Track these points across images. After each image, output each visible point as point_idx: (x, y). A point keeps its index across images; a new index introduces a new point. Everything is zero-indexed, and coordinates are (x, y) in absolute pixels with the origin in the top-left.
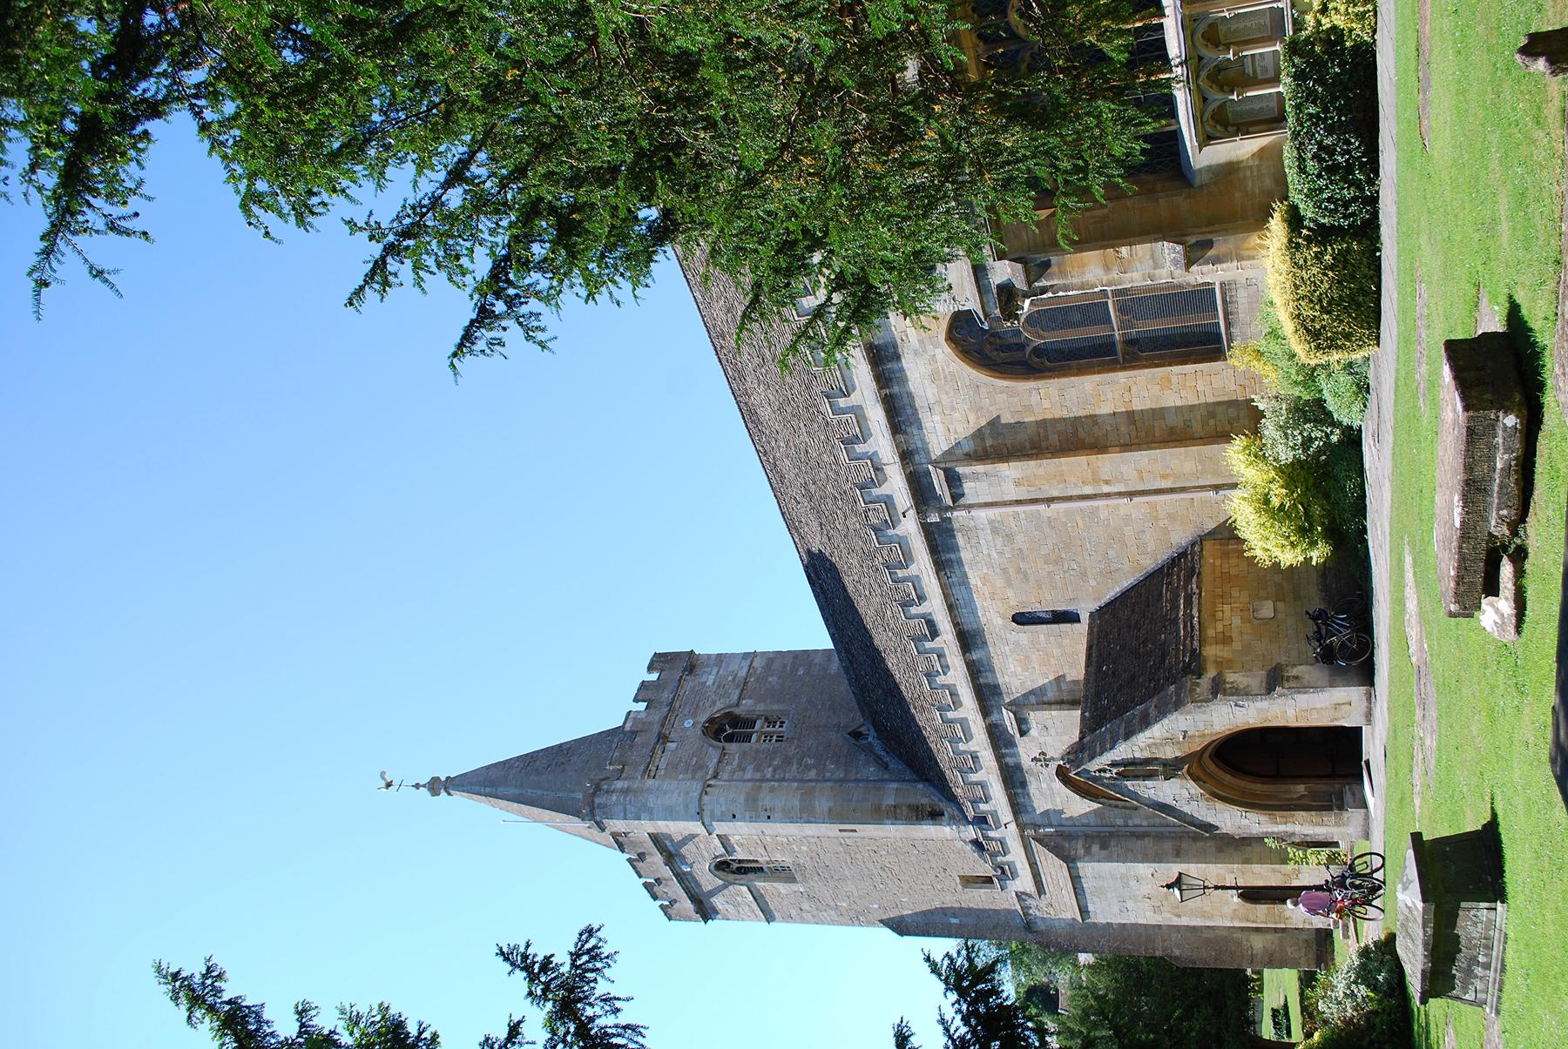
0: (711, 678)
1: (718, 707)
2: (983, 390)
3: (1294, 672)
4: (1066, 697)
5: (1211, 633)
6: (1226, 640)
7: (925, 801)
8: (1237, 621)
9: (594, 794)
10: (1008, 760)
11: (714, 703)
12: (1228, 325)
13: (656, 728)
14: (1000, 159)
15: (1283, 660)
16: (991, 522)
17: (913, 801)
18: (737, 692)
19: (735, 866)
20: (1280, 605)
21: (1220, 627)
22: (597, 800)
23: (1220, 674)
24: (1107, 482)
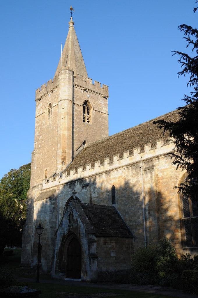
0: (101, 103)
1: (92, 104)
2: (175, 180)
3: (96, 261)
4: (93, 199)
5: (107, 239)
6: (105, 243)
7: (67, 160)
8: (110, 246)
9: (69, 70)
10: (76, 183)
11: (94, 103)
12: (151, 121)
13: (87, 87)
14: (184, 109)
15: (99, 258)
16: (139, 181)
17: (67, 157)
18: (97, 110)
19: (50, 109)
20: (114, 258)
21: (109, 242)
22: (67, 71)
23: (95, 242)
24: (149, 213)
